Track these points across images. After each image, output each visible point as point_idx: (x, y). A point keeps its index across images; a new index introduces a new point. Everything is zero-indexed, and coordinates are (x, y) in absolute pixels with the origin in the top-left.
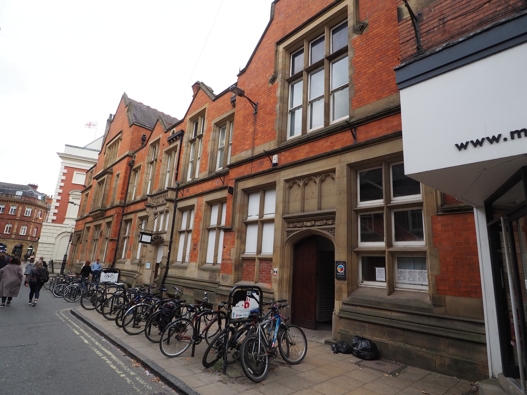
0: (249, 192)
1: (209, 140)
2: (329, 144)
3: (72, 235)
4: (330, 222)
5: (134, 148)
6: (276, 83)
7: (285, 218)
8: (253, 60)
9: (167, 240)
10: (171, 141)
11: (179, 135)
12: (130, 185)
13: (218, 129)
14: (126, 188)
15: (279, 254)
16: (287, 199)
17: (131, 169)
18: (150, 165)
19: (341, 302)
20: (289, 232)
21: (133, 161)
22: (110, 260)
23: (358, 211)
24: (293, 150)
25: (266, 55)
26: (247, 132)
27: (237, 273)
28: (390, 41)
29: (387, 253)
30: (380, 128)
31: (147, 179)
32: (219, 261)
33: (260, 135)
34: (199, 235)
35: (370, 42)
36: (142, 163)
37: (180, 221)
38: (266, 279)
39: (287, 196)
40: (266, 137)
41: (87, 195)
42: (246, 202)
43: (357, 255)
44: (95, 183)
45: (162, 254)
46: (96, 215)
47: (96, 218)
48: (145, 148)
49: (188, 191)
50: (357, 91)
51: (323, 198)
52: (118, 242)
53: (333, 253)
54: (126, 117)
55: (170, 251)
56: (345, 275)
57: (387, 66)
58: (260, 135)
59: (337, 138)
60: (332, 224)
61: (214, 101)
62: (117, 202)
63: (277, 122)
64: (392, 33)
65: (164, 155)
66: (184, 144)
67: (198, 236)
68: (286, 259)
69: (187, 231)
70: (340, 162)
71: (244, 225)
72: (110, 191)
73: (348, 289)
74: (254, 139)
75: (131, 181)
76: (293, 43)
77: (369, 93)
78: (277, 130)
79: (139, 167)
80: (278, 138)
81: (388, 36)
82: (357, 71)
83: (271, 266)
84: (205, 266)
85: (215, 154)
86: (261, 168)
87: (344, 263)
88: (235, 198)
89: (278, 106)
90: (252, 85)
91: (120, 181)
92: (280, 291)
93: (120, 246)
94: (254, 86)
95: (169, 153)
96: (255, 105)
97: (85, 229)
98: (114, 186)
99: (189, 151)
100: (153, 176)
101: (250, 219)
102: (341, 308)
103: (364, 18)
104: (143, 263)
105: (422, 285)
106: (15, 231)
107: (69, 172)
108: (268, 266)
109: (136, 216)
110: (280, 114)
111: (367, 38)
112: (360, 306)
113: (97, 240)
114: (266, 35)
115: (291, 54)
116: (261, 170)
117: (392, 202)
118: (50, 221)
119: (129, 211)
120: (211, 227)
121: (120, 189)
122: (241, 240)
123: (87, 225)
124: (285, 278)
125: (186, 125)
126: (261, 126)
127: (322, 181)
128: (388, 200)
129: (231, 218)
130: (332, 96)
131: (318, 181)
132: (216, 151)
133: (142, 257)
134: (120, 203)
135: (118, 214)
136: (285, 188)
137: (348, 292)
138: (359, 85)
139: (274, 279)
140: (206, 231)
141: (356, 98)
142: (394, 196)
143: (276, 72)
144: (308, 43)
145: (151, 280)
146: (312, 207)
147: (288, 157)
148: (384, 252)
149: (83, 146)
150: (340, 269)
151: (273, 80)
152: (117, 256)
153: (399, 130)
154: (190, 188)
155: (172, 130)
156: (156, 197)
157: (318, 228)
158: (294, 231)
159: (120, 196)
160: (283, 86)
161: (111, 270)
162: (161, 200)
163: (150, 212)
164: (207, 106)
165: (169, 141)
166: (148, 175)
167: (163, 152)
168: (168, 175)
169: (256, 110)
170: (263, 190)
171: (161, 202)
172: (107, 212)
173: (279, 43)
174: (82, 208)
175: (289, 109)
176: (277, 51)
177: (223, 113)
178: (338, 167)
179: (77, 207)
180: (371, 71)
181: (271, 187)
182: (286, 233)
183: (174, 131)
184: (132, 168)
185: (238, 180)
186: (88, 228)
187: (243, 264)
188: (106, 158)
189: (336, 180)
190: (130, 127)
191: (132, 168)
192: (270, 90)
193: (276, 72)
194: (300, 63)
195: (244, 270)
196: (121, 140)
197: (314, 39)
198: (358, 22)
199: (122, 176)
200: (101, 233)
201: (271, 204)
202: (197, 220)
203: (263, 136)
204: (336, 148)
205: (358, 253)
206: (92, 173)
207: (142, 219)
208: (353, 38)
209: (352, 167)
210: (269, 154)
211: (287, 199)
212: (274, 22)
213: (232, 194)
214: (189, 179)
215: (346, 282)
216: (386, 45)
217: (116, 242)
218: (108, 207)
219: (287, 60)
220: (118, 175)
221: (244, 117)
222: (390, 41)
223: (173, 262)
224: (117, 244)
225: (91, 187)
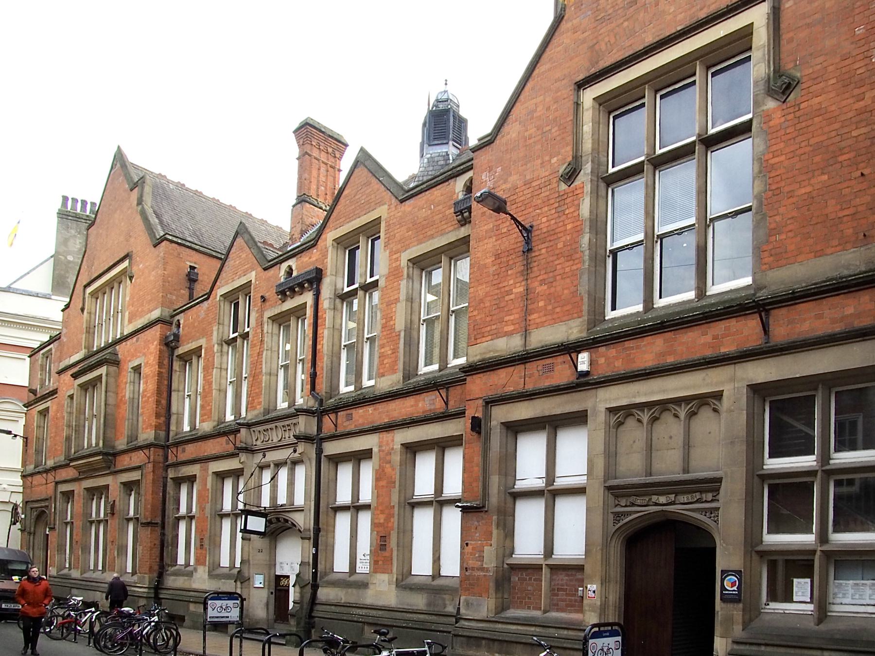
0: (516, 429)
1: (397, 300)
2: (708, 338)
3: (15, 507)
4: (710, 496)
5: (172, 302)
6: (577, 183)
7: (609, 488)
8: (513, 116)
10: (286, 291)
11: (310, 282)
12: (174, 395)
13: (417, 272)
14: (164, 402)
15: (599, 557)
16: (612, 449)
19: (730, 640)
20: (618, 516)
21: (177, 337)
22: (151, 567)
23: (764, 478)
24: (627, 344)
25: (548, 109)
26: (509, 293)
27: (500, 595)
28: (846, 130)
29: (818, 553)
30: (819, 317)
31: (223, 381)
32: (238, 565)
33: (541, 304)
34: (391, 516)
35: (804, 124)
36: (202, 342)
37: (332, 484)
38: (567, 606)
39: (613, 440)
40: (558, 310)
41: (44, 413)
42: (510, 450)
43: (761, 557)
45: (290, 558)
46: (89, 464)
47: (88, 472)
49: (349, 417)
50: (772, 232)
51: (692, 451)
52: (163, 527)
53: (711, 553)
54: (138, 218)
55: (317, 551)
56: (739, 595)
57: (840, 186)
58: (541, 304)
59: (727, 328)
60: (712, 501)
61: (402, 201)
62: (147, 435)
63: (585, 277)
64: (850, 115)
66: (325, 304)
68: (612, 566)
70: (733, 379)
71: (509, 499)
72: (117, 406)
73: (743, 619)
74: (527, 312)
75: (174, 386)
76: (607, 76)
77: (798, 239)
78: (586, 300)
80: (589, 314)
81: (843, 118)
82: (773, 187)
83: (582, 580)
84: (410, 581)
85: (415, 333)
86: (547, 378)
87: (738, 573)
88: (487, 440)
89: (585, 239)
90: (514, 179)
91: (148, 386)
93: (169, 537)
94: (520, 183)
96: (527, 231)
97: (59, 496)
99: (338, 321)
101: (520, 485)
102: (729, 649)
103: (792, 65)
104: (246, 575)
105: (544, 626)
108: (571, 580)
109: (206, 470)
110: (590, 259)
111: (798, 114)
112: (766, 645)
113: (99, 522)
114: (545, 56)
115: (610, 113)
116: (546, 383)
117: (832, 462)
119: (182, 457)
120: (416, 499)
122: (504, 530)
124: (611, 603)
125: (325, 256)
126: (542, 282)
127: (692, 414)
128: (825, 458)
129: (480, 484)
130: (711, 228)
131: (682, 414)
134: (155, 439)
135: (155, 463)
136: (607, 424)
137: (744, 622)
138: (778, 218)
139: (590, 605)
140: (407, 507)
141: (771, 247)
142: (837, 450)
144: (653, 94)
145: (268, 609)
146: (668, 465)
147: (612, 360)
148: (814, 552)
150: (730, 584)
151: (570, 176)
152: (167, 560)
154: (353, 411)
155: (284, 266)
156: (261, 428)
157: (682, 507)
158: (630, 513)
159: (153, 421)
160: (596, 195)
164: (381, 212)
166: (224, 373)
167: (265, 319)
168: (95, 420)
169: (527, 243)
170: (552, 425)
171: (275, 440)
175: (609, 248)
176: (577, 105)
177: (432, 237)
178: (728, 390)
179: (20, 442)
180: (803, 191)
181: (578, 419)
182: (611, 517)
183: (290, 268)
184: (174, 354)
185: (491, 402)
186: (68, 496)
187: (513, 577)
188: (89, 322)
189: (724, 415)
190: (155, 246)
191: (174, 354)
192: (562, 198)
194: (632, 137)
195: (514, 588)
196: (131, 278)
197: (669, 86)
198: (778, 72)
200: (113, 506)
201: (575, 455)
202: (382, 483)
203: (550, 307)
204: (724, 350)
205: (762, 554)
206: (47, 356)
208: (765, 108)
209: (757, 390)
210: (570, 349)
211: (612, 449)
212: (564, 26)
213: (479, 433)
214: (345, 389)
215: (741, 605)
216: (838, 138)
217: (159, 529)
218: (121, 444)
220: (137, 369)
221: (498, 256)
222: (846, 130)
223: (325, 574)
224: (163, 534)
225: (54, 392)
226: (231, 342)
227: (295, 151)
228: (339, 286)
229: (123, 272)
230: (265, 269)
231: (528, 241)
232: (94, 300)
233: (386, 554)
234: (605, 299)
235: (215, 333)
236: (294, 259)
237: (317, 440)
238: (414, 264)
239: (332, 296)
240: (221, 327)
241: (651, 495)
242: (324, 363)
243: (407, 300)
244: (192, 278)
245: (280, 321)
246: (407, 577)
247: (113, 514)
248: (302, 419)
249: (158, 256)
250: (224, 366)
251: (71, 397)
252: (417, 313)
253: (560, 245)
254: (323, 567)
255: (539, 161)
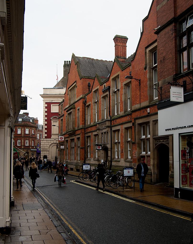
3: (57, 145)
6: (146, 70)
9: (109, 148)
10: (104, 92)
13: (126, 87)
16: (154, 129)
17: (85, 105)
18: (95, 104)
20: (156, 144)
21: (86, 102)
22: (83, 159)
31: (95, 112)
34: (123, 145)
36: (90, 103)
41: (62, 120)
44: (66, 114)
46: (70, 133)
47: (71, 135)
48: (91, 93)
62: (81, 126)
65: (102, 100)
66: (111, 94)
67: (123, 146)
69: (118, 143)
72: (75, 119)
74: (140, 99)
79: (90, 105)
80: (149, 100)
84: (128, 160)
85: (126, 102)
88: (135, 127)
91: (80, 114)
92: (154, 169)
95: (104, 97)
98: (77, 116)
99: (114, 98)
100: (98, 111)
106: (23, 144)
107: (48, 106)
109: (92, 134)
110: (149, 87)
113: (73, 148)
118: (44, 137)
121: (81, 119)
123: (66, 139)
132: (127, 100)
133: (98, 156)
143: (146, 65)
149: (52, 87)
151: (145, 68)
152: (86, 157)
153: (157, 119)
154: (116, 120)
156: (101, 124)
158: (157, 144)
160: (150, 72)
161: (85, 163)
162: (104, 126)
163: (99, 132)
165: (103, 92)
166: (95, 110)
172: (76, 132)
173: (146, 48)
174: (60, 128)
176: (146, 52)
182: (154, 144)
184: (86, 106)
185: (135, 119)
186: (67, 141)
190: (80, 79)
193: (146, 65)
199: (81, 110)
200: (75, 144)
202: (122, 137)
203: (144, 98)
207: (95, 135)
211: (154, 129)
219: (151, 57)
223: (114, 159)
225: (63, 115)
226: (96, 102)
227: (114, 44)
228: (114, 89)
229: (75, 85)
230: (101, 85)
231: (140, 83)
232: (70, 92)
233: (123, 154)
234: (153, 95)
235: (93, 100)
236: (105, 83)
237: (110, 127)
238: (125, 85)
239: (112, 92)
240: (94, 99)
241: (160, 140)
242: (111, 108)
243: (124, 94)
244: (89, 86)
245: (131, 78)
246: (127, 159)
247: (75, 146)
248: (107, 122)
249: (81, 82)
250: (95, 108)
251: (66, 116)
252: (127, 97)
253: (145, 84)
254: (113, 157)
255: (141, 65)
